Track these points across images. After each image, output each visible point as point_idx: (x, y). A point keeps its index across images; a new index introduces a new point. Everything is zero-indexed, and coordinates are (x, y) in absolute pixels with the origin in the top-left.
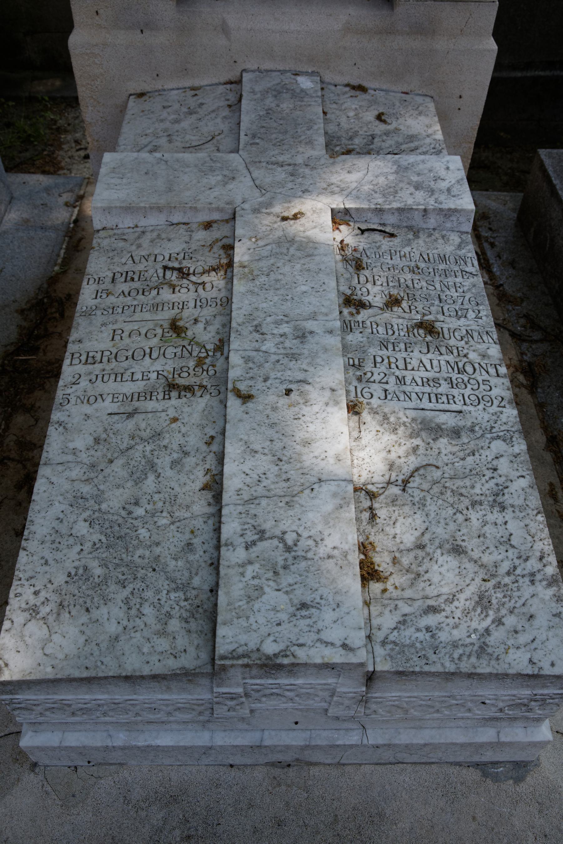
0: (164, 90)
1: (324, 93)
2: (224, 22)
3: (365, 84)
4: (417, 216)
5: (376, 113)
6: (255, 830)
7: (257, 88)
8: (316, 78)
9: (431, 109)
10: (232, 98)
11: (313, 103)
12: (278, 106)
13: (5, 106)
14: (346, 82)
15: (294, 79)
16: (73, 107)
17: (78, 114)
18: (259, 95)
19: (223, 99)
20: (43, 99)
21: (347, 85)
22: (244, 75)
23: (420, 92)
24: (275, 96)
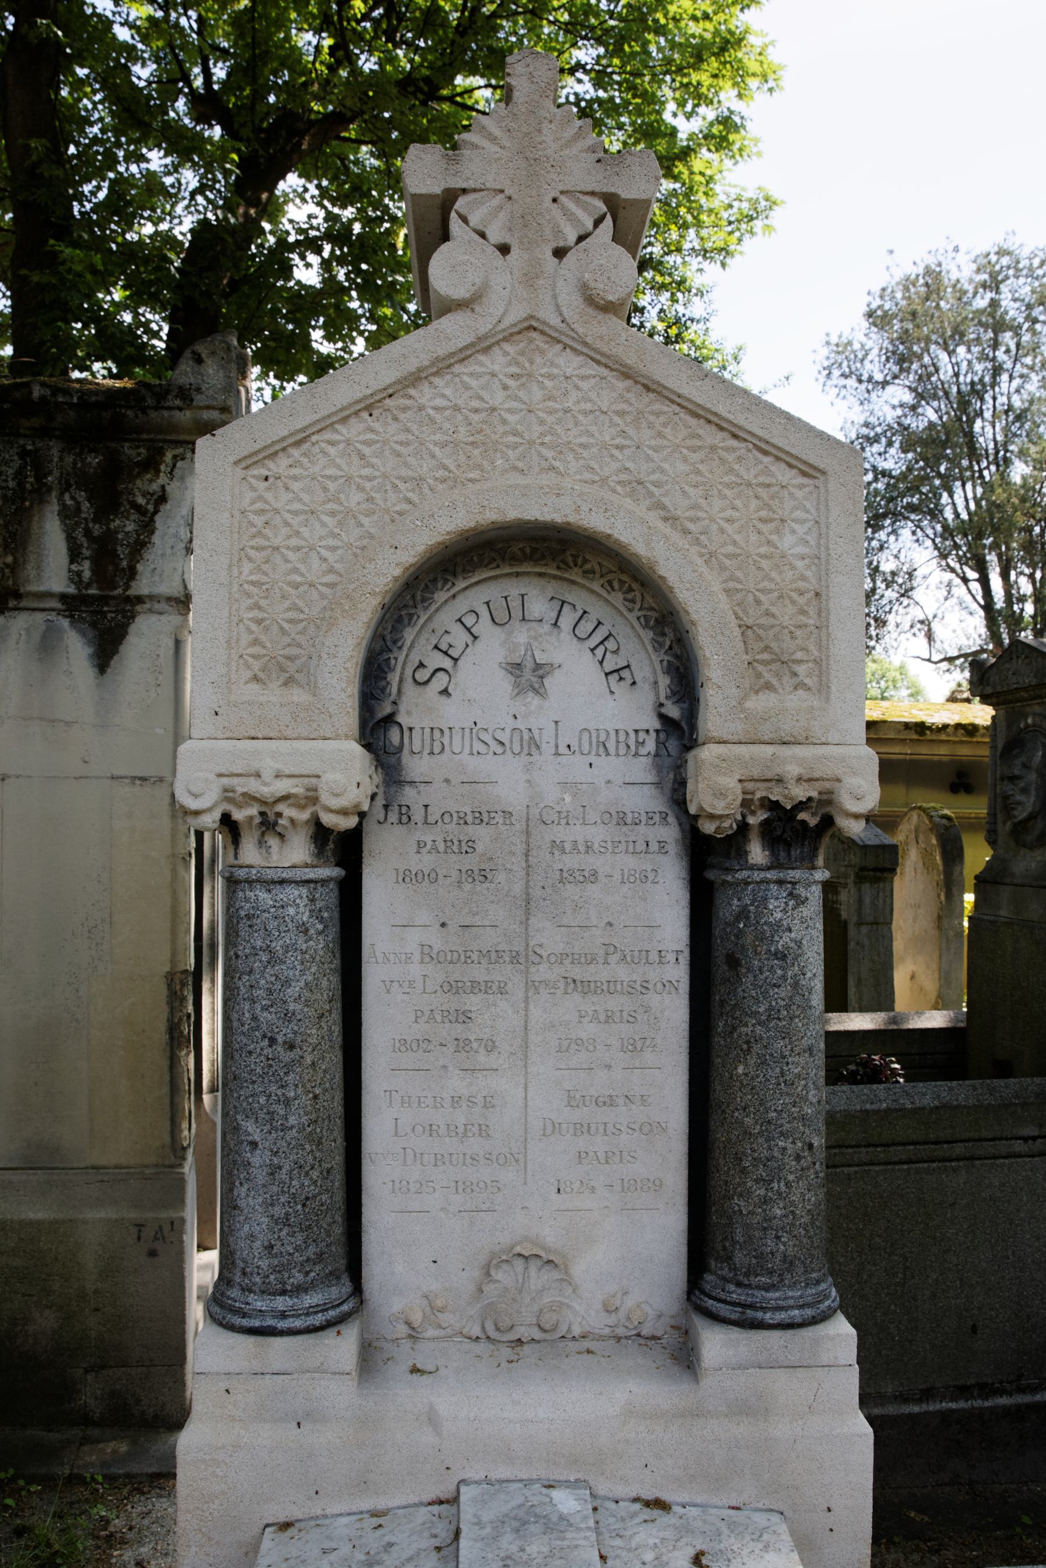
0: (325, 1517)
1: (598, 1517)
2: (432, 1407)
3: (665, 1496)
5: (691, 1552)
7: (487, 1516)
8: (583, 1491)
9: (783, 1537)
10: (444, 1533)
11: (582, 1542)
12: (523, 1550)
13: (24, 1493)
14: (634, 1495)
15: (547, 1495)
16: (143, 1493)
17: (150, 1507)
18: (488, 1530)
19: (426, 1534)
20: (93, 1478)
21: (636, 1500)
22: (463, 1489)
23: (760, 1506)
24: (517, 1531)
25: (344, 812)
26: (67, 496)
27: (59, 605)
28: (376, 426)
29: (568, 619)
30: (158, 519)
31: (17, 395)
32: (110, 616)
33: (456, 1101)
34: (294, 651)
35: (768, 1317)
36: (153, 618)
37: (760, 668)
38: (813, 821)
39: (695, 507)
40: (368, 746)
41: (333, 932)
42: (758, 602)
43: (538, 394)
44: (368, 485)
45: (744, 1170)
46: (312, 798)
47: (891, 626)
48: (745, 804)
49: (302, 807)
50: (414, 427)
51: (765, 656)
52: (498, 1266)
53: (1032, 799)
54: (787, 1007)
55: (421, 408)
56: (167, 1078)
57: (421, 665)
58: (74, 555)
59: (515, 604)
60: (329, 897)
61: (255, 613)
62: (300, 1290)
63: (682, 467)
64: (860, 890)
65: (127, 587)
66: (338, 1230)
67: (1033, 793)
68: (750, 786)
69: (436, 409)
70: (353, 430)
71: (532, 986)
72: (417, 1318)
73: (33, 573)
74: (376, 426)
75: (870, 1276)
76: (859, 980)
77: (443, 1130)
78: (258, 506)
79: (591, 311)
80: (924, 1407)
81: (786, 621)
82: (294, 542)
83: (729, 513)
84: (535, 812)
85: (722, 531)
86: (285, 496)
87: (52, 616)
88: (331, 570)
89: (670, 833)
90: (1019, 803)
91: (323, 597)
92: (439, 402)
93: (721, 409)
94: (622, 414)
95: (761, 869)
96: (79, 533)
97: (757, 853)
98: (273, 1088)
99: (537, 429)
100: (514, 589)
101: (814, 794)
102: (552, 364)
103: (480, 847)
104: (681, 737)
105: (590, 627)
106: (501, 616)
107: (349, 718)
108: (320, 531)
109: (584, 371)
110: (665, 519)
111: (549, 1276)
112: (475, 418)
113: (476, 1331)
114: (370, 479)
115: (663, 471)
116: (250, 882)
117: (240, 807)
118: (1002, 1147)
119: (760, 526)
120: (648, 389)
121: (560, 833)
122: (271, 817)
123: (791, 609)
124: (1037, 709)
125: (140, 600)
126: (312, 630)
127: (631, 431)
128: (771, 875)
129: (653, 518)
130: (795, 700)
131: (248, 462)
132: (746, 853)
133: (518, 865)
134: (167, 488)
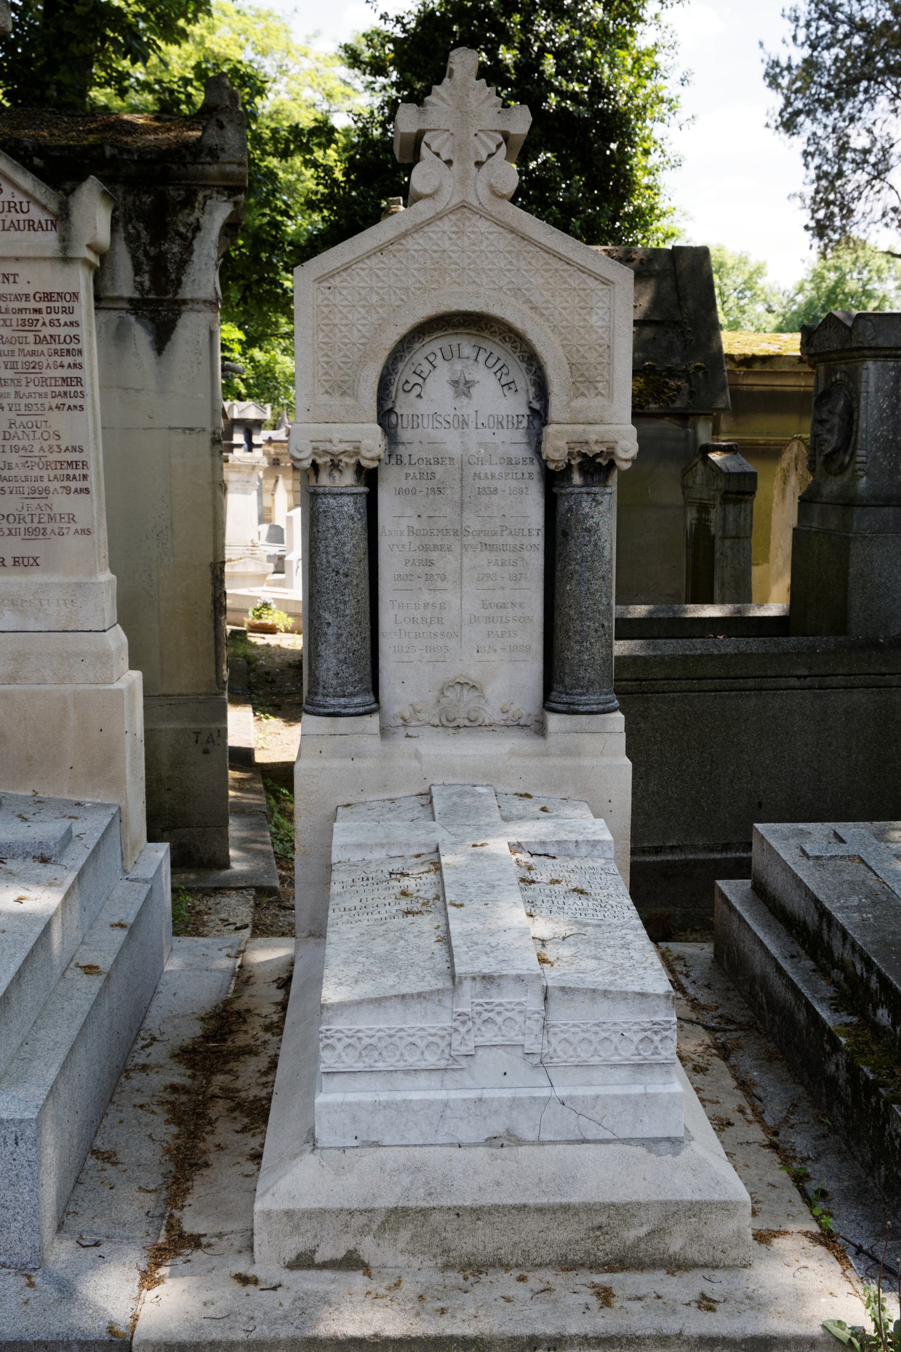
2: (417, 750)
3: (529, 792)
4: (572, 847)
6: (480, 1189)
22: (433, 788)
25: (372, 459)
26: (130, 227)
27: (127, 306)
28: (385, 260)
29: (482, 357)
30: (196, 244)
31: (95, 153)
32: (164, 313)
33: (426, 605)
34: (346, 378)
35: (581, 708)
36: (194, 315)
37: (579, 385)
38: (604, 463)
39: (547, 301)
40: (380, 424)
41: (365, 520)
42: (578, 351)
43: (467, 242)
44: (381, 292)
45: (569, 637)
46: (357, 452)
47: (857, 216)
48: (570, 454)
49: (351, 457)
50: (404, 261)
51: (582, 379)
52: (447, 689)
53: (836, 437)
54: (591, 556)
55: (407, 250)
56: (212, 635)
57: (407, 382)
58: (137, 270)
59: (455, 349)
60: (362, 502)
61: (326, 359)
62: (352, 695)
63: (541, 280)
64: (724, 509)
65: (176, 293)
66: (369, 669)
67: (836, 432)
68: (572, 445)
69: (415, 251)
70: (373, 262)
71: (464, 547)
72: (407, 715)
73: (109, 283)
74: (385, 260)
75: (688, 767)
76: (723, 584)
77: (419, 621)
78: (326, 302)
79: (494, 198)
80: (724, 855)
81: (593, 361)
82: (344, 322)
83: (565, 304)
84: (466, 458)
85: (560, 314)
86: (339, 298)
87: (123, 314)
88: (364, 336)
89: (535, 469)
90: (826, 441)
91: (359, 350)
92: (417, 247)
93: (561, 250)
94: (510, 252)
95: (578, 487)
96: (140, 254)
97: (577, 479)
98: (338, 596)
99: (467, 261)
100: (454, 341)
101: (604, 449)
102: (475, 226)
103: (438, 476)
104: (541, 419)
105: (494, 361)
106: (448, 355)
107: (373, 414)
108: (357, 315)
109: (491, 230)
110: (532, 308)
111: (474, 694)
112: (435, 255)
113: (437, 722)
114: (382, 288)
115: (531, 283)
116: (325, 494)
117: (320, 457)
118: (782, 682)
119: (581, 311)
120: (523, 239)
121: (478, 469)
122: (336, 462)
123: (595, 354)
124: (843, 367)
125: (184, 302)
126: (355, 367)
127: (515, 261)
128: (583, 490)
129: (525, 308)
130: (596, 402)
131: (320, 280)
132: (572, 479)
133: (457, 485)
134: (201, 220)
